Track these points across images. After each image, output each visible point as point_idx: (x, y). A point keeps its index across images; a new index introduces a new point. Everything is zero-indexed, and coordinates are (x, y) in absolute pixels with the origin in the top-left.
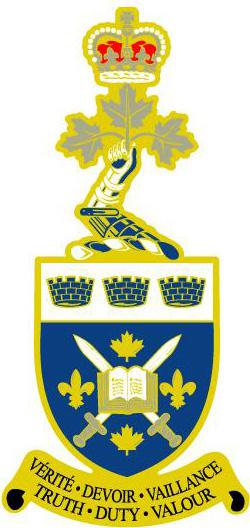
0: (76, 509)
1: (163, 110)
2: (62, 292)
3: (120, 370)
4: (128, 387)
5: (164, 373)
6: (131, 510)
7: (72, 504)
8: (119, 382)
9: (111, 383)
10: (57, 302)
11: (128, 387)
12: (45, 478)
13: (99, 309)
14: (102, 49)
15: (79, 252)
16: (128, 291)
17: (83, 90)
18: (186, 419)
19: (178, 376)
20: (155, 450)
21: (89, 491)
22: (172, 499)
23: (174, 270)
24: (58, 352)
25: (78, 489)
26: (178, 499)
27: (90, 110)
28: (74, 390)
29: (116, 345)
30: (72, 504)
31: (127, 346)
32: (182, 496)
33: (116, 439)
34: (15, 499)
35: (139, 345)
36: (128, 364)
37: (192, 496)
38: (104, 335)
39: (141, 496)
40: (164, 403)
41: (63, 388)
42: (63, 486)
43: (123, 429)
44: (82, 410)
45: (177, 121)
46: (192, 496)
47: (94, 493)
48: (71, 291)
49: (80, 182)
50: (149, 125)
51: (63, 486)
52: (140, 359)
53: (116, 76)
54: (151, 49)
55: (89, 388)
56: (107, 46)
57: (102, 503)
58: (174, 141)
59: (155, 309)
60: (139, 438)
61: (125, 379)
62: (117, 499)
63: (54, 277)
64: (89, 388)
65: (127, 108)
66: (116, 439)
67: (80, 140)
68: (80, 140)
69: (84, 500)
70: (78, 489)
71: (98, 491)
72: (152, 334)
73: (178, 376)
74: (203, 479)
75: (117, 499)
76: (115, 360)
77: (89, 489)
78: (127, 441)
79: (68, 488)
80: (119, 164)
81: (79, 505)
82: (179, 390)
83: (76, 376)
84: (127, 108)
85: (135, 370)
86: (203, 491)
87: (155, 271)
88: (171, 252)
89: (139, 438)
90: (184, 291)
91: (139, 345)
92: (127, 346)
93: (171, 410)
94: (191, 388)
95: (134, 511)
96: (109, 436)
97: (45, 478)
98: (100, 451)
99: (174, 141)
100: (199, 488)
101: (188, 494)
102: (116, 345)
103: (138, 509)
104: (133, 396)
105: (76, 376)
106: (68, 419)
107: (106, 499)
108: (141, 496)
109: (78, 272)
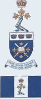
0: (16, 68)
1: (26, 12)
3: (20, 48)
4: (21, 49)
11: (21, 49)
13: (17, 39)
16: (21, 36)
18: (29, 54)
20: (25, 58)
23: (28, 33)
24: (12, 45)
28: (14, 50)
34: (6, 66)
36: (21, 46)
38: (18, 42)
48: (13, 37)
49: (16, 21)
50: (25, 14)
52: (23, 46)
58: (24, 87)
59: (25, 39)
67: (16, 16)
68: (16, 16)
83: (28, 51)
88: (27, 31)
90: (29, 36)
92: (21, 44)
98: (17, 58)
99: (24, 87)
106: (13, 54)
109: (15, 34)
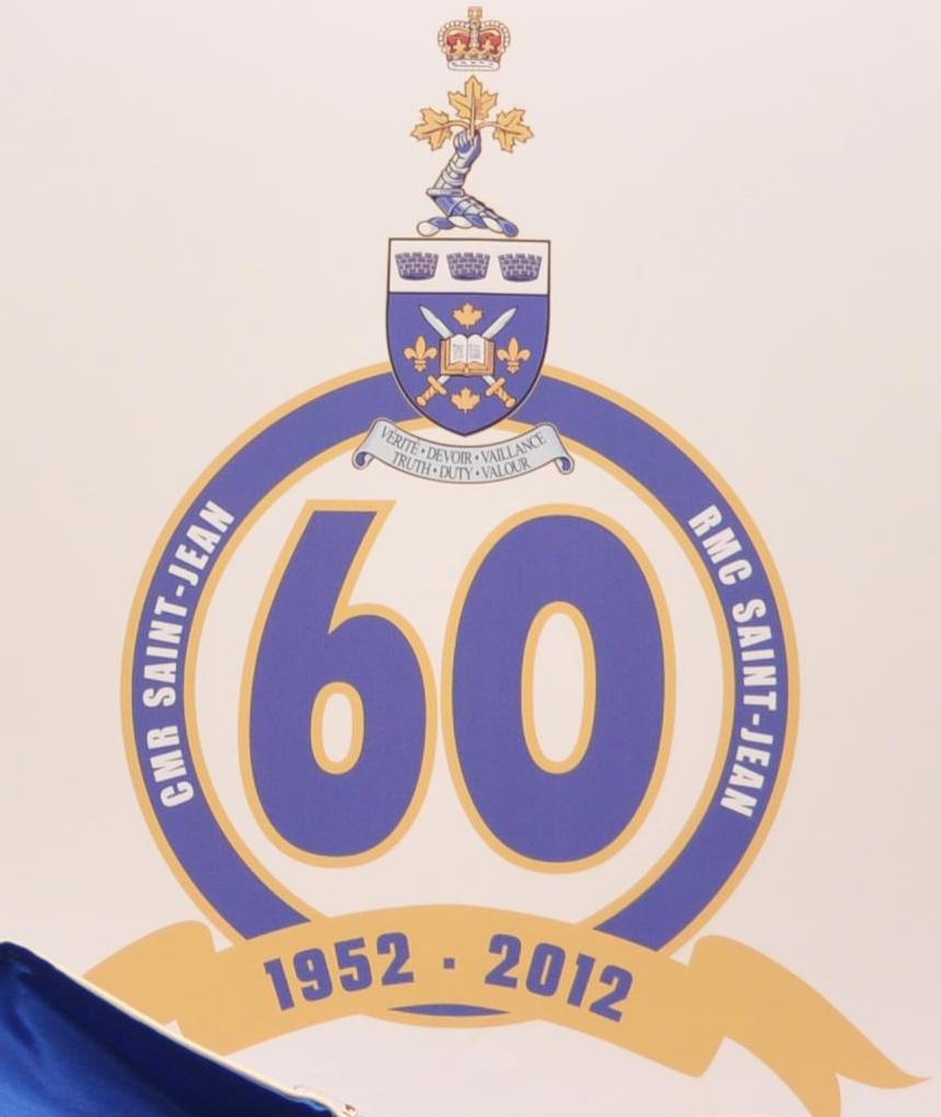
2: (404, 261)
3: (459, 339)
5: (499, 342)
8: (459, 347)
13: (443, 281)
14: (451, 42)
15: (427, 229)
16: (469, 267)
19: (514, 344)
21: (445, 470)
23: (513, 249)
25: (423, 451)
29: (458, 315)
31: (468, 316)
33: (455, 399)
35: (478, 315)
36: (468, 332)
38: (445, 304)
39: (477, 458)
41: (409, 353)
42: (410, 449)
44: (425, 373)
45: (519, 113)
48: (418, 267)
51: (410, 449)
52: (479, 329)
54: (497, 42)
55: (432, 353)
56: (473, 82)
57: (444, 463)
59: (494, 282)
60: (476, 399)
61: (465, 344)
63: (401, 252)
64: (432, 353)
65: (475, 102)
66: (455, 399)
67: (432, 130)
68: (432, 130)
69: (428, 461)
70: (423, 451)
72: (490, 304)
73: (514, 344)
76: (457, 328)
80: (465, 148)
81: (427, 466)
83: (421, 343)
84: (475, 102)
85: (475, 339)
87: (496, 250)
88: (510, 231)
89: (476, 399)
90: (520, 269)
91: (478, 315)
92: (468, 316)
93: (507, 375)
94: (525, 354)
96: (448, 397)
102: (458, 315)
105: (421, 343)
107: (447, 459)
108: (477, 458)
109: (424, 248)
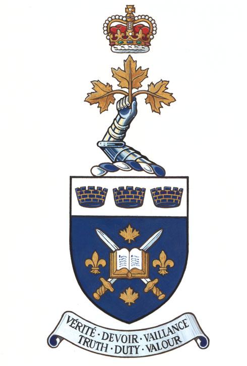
1: (154, 77)
4: (129, 260)
6: (136, 346)
7: (100, 345)
9: (118, 258)
10: (83, 204)
11: (129, 260)
12: (76, 329)
13: (110, 208)
15: (96, 172)
17: (105, 62)
18: (170, 282)
19: (163, 255)
20: (148, 305)
22: (156, 341)
23: (161, 183)
24: (85, 238)
26: (160, 341)
27: (107, 78)
28: (94, 261)
30: (100, 345)
32: (162, 340)
34: (53, 341)
37: (168, 340)
38: (113, 225)
40: (153, 272)
43: (127, 290)
46: (168, 340)
47: (110, 337)
53: (123, 48)
59: (148, 209)
62: (124, 341)
65: (132, 75)
66: (123, 297)
67: (100, 97)
68: (100, 97)
71: (112, 336)
72: (145, 225)
73: (163, 255)
74: (178, 330)
75: (124, 341)
77: (106, 335)
78: (129, 297)
79: (93, 335)
82: (163, 262)
84: (132, 75)
86: (175, 338)
87: (150, 184)
88: (160, 172)
90: (167, 198)
92: (129, 234)
93: (114, 36)
95: (137, 347)
97: (76, 329)
98: (109, 304)
100: (174, 336)
101: (165, 339)
103: (139, 346)
104: (134, 267)
105: (95, 256)
106: (87, 281)
107: (117, 341)
